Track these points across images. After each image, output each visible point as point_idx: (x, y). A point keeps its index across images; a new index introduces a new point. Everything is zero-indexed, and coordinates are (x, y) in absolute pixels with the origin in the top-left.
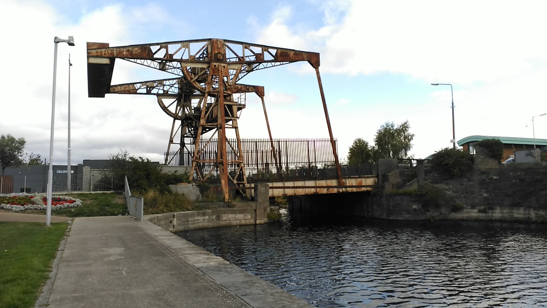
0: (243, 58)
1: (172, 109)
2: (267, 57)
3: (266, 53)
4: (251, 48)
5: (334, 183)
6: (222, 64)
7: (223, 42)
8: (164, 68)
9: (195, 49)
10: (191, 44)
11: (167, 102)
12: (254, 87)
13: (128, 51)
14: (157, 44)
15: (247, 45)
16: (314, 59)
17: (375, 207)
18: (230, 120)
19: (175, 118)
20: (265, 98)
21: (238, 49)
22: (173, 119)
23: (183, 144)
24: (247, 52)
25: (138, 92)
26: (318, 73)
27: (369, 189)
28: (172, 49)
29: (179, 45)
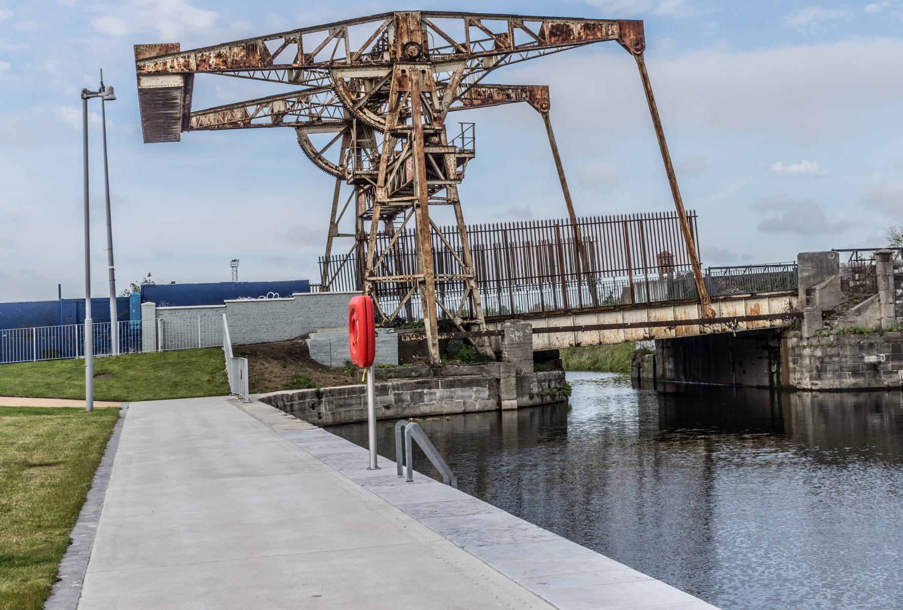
0: (463, 46)
1: (333, 156)
3: (518, 32)
4: (485, 23)
5: (692, 312)
6: (417, 67)
8: (301, 78)
9: (359, 38)
10: (351, 30)
11: (318, 139)
12: (523, 89)
13: (219, 56)
14: (280, 36)
15: (472, 18)
16: (632, 36)
17: (791, 365)
18: (440, 187)
19: (341, 178)
20: (551, 113)
21: (456, 29)
22: (335, 179)
23: (362, 238)
24: (476, 34)
25: (253, 122)
26: (641, 65)
27: (778, 322)
28: (311, 42)
29: (325, 34)
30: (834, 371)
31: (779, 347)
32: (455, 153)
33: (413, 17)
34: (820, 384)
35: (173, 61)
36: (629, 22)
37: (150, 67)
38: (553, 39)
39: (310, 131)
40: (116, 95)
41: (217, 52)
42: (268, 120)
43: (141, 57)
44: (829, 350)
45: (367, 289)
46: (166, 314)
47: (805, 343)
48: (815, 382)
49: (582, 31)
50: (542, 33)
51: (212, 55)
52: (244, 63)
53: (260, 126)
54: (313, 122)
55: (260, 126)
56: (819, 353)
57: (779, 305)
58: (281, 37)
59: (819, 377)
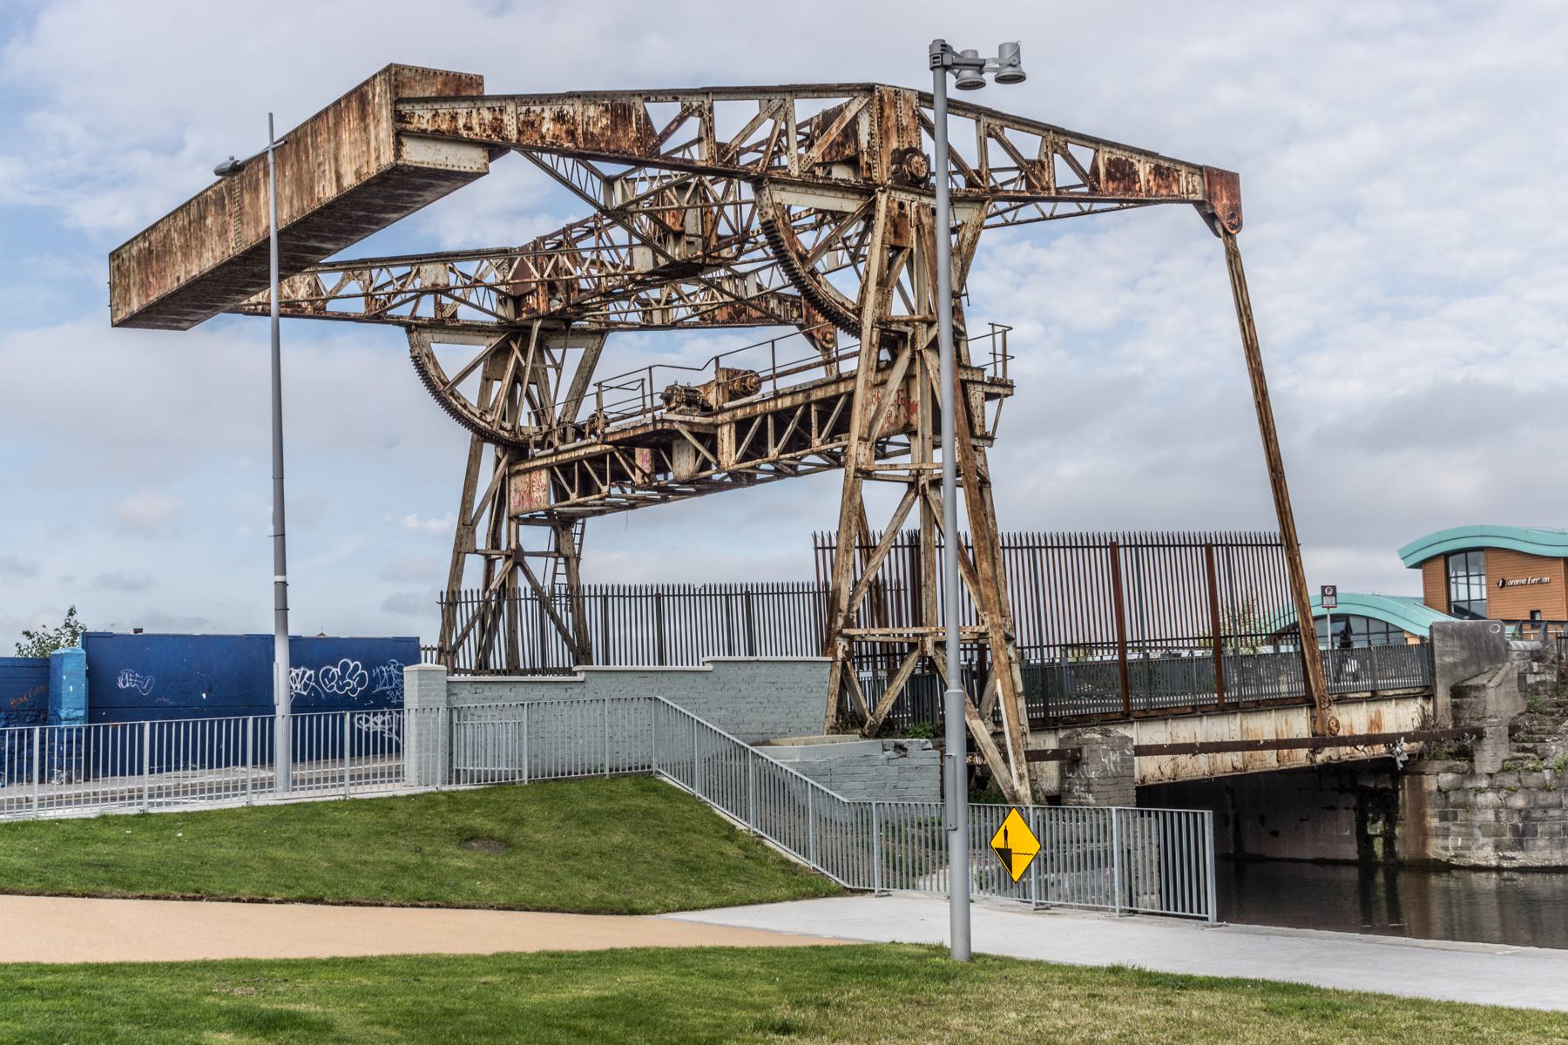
2: (1063, 175)
5: (1298, 724)
7: (915, 102)
11: (453, 356)
13: (560, 118)
14: (674, 95)
15: (995, 123)
16: (1218, 200)
25: (332, 306)
26: (1233, 257)
30: (1552, 835)
31: (1396, 791)
32: (982, 383)
33: (907, 101)
34: (1521, 858)
35: (469, 114)
36: (1222, 173)
37: (423, 118)
38: (1111, 185)
39: (437, 337)
40: (1025, 67)
41: (556, 108)
42: (358, 307)
43: (406, 93)
44: (1541, 795)
45: (840, 655)
46: (465, 693)
47: (1484, 783)
48: (1509, 854)
49: (1151, 178)
50: (1095, 168)
51: (547, 114)
52: (608, 143)
53: (344, 317)
54: (443, 320)
55: (344, 317)
56: (1519, 801)
57: (1401, 717)
58: (676, 99)
59: (1519, 844)
